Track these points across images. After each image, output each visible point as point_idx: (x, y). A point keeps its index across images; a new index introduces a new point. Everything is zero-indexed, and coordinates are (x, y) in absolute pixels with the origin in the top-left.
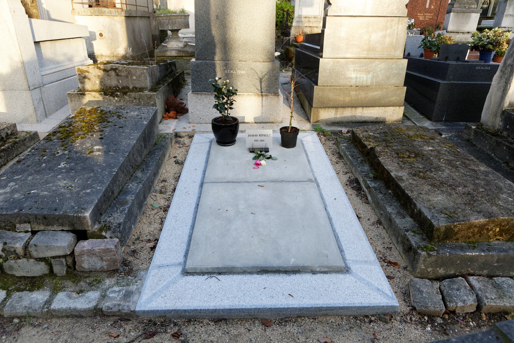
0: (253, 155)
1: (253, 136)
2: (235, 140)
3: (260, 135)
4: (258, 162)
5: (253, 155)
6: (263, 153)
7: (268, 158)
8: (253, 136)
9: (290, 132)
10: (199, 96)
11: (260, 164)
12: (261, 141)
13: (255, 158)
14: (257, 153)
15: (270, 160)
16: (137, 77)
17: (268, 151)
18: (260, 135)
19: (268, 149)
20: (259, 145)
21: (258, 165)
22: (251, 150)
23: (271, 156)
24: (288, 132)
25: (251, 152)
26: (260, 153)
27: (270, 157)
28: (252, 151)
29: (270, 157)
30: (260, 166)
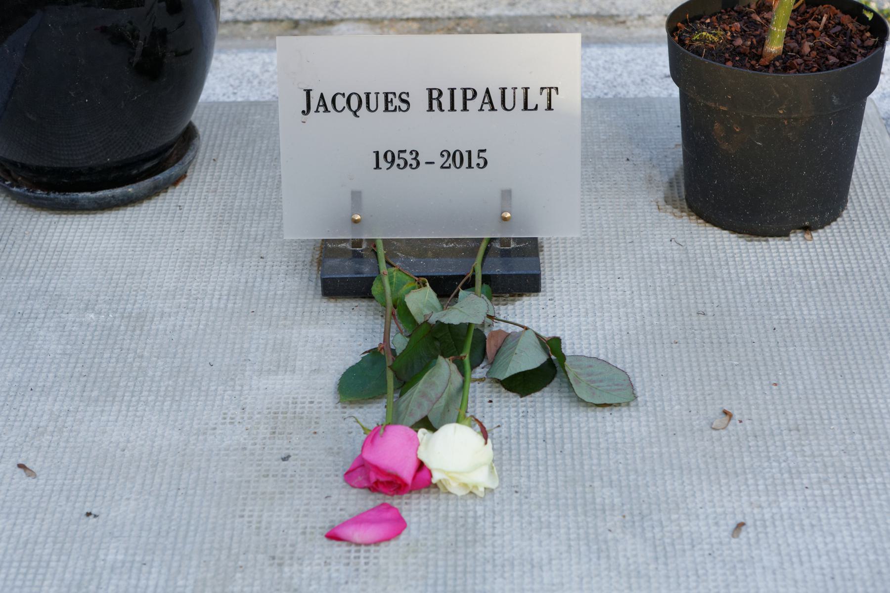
0: (348, 333)
1: (357, 103)
2: (189, 135)
3: (434, 98)
4: (393, 455)
5: (348, 333)
6: (469, 309)
7: (524, 384)
8: (357, 103)
9: (786, 62)
10: (136, 208)
11: (422, 478)
12: (455, 159)
13: (363, 382)
14: (401, 310)
15: (545, 403)
16: (838, 56)
17: (530, 284)
18: (434, 98)
19: (531, 248)
20: (437, 205)
21: (390, 485)
22: (345, 269)
23: (552, 345)
24: (752, 56)
25: (333, 289)
26: (437, 312)
27: (547, 372)
28: (345, 273)
29: (547, 372)
30: (412, 508)
